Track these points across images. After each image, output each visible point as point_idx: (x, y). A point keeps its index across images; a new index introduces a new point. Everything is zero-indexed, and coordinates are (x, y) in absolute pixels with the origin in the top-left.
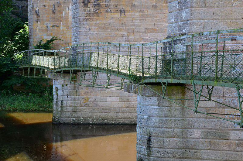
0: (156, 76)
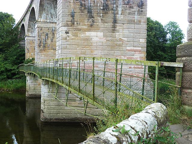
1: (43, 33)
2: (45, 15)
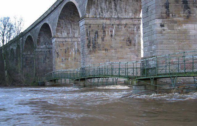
0: (170, 73)
1: (92, 31)
2: (94, 10)
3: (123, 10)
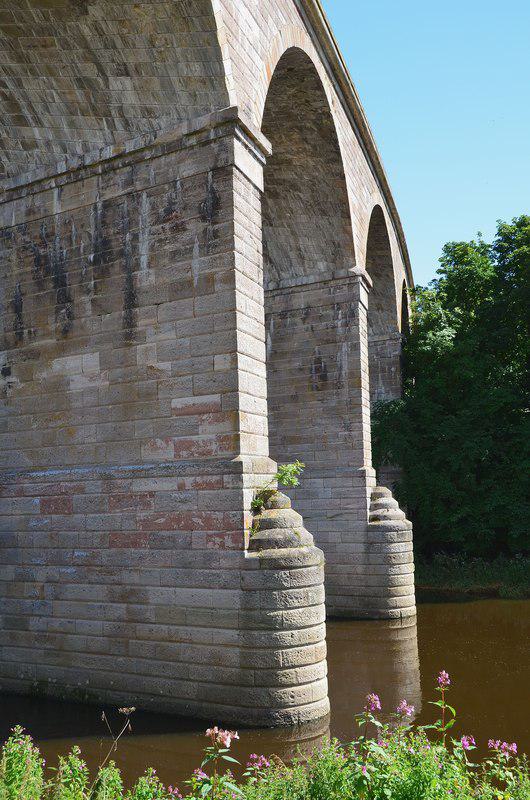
3: (293, 255)
